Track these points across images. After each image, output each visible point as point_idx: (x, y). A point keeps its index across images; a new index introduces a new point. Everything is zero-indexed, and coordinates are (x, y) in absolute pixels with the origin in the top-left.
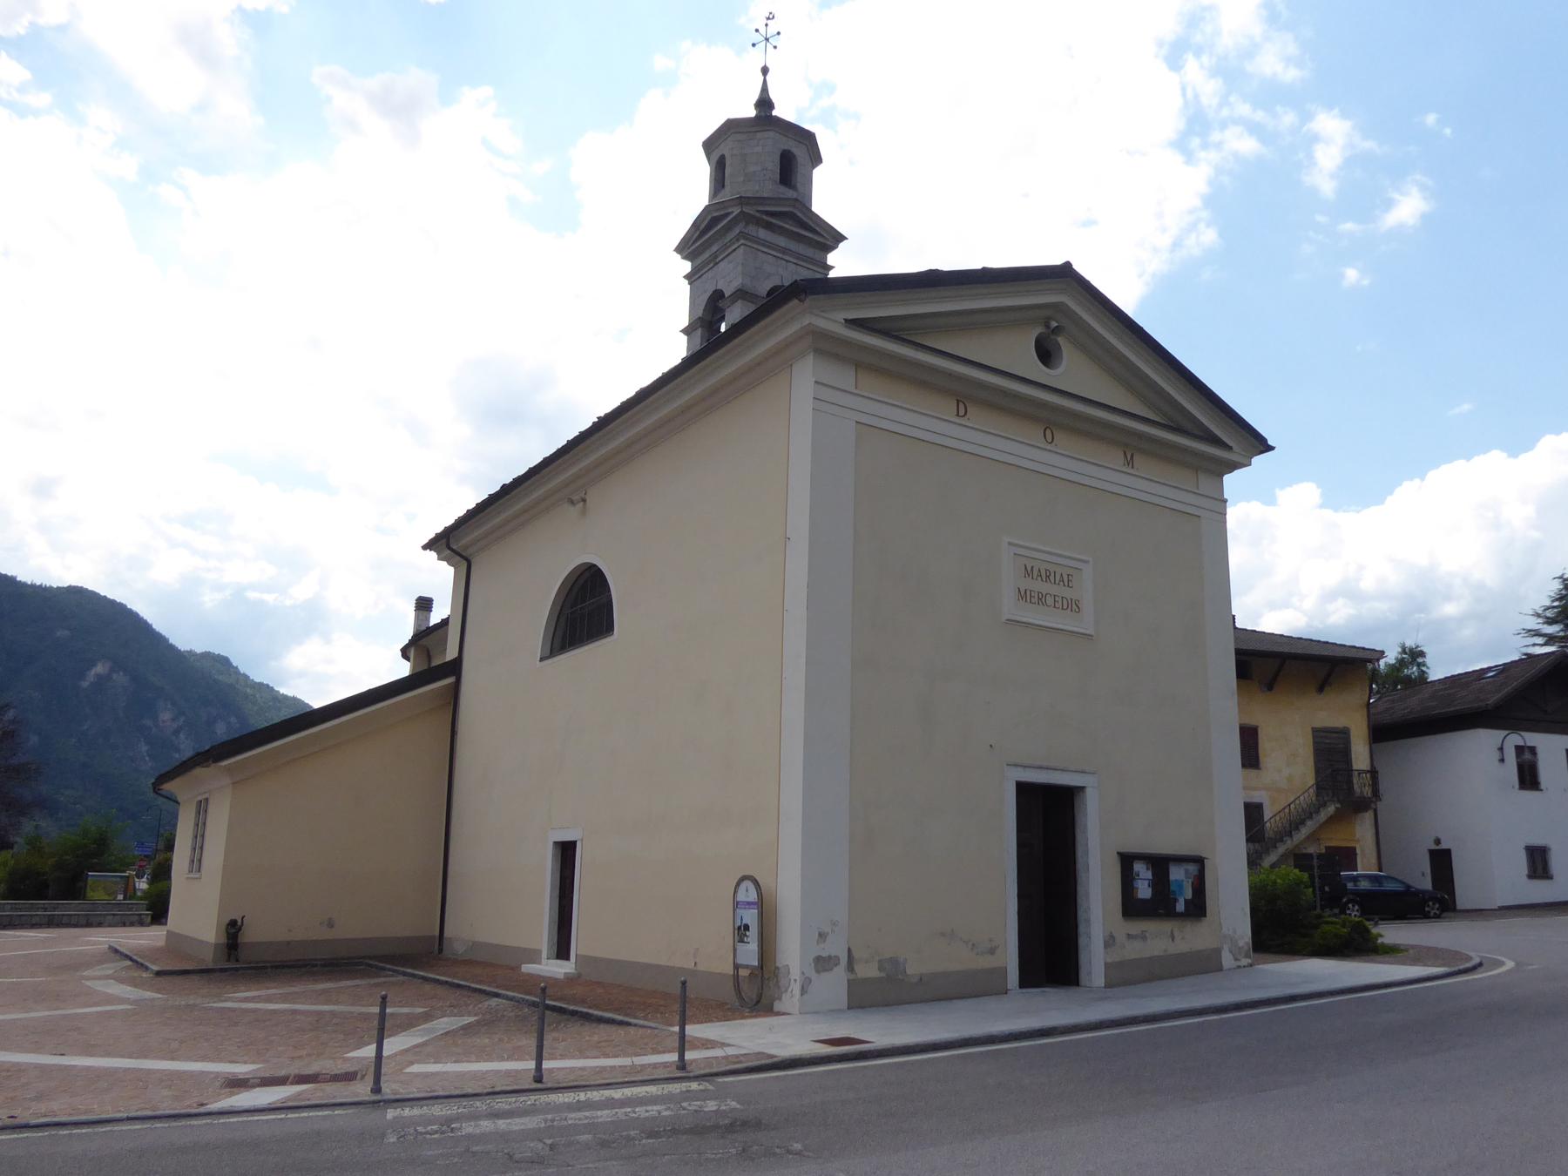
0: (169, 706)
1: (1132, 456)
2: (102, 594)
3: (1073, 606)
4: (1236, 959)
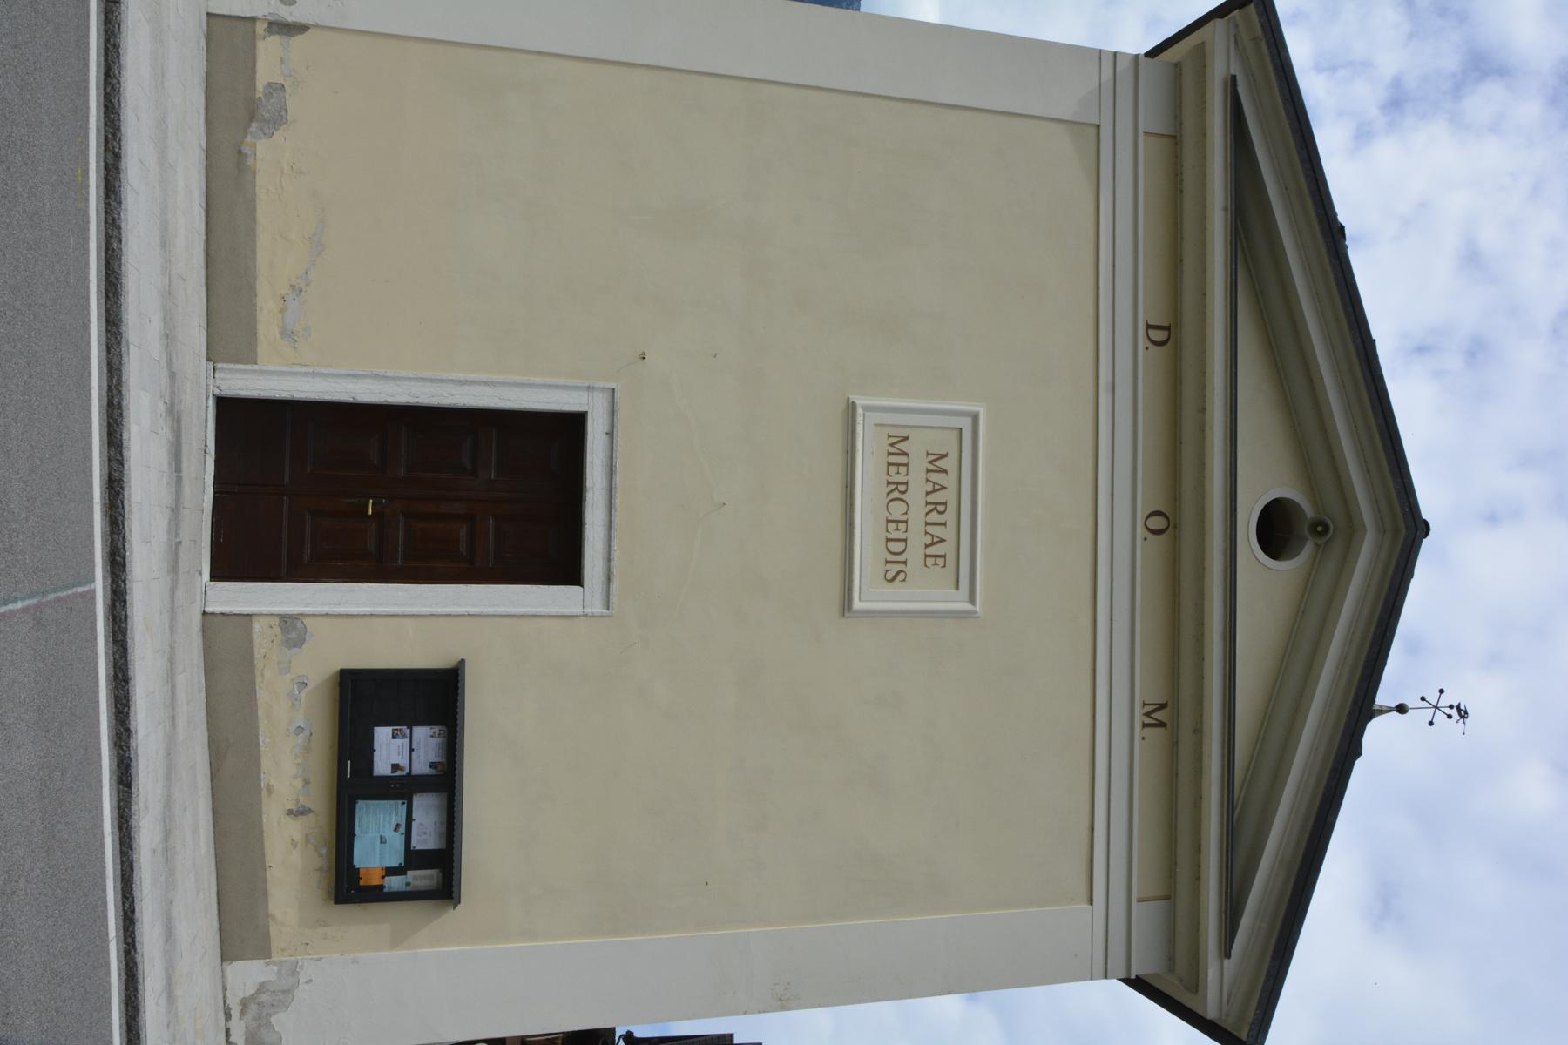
1: (1161, 724)
3: (895, 570)
4: (245, 1004)
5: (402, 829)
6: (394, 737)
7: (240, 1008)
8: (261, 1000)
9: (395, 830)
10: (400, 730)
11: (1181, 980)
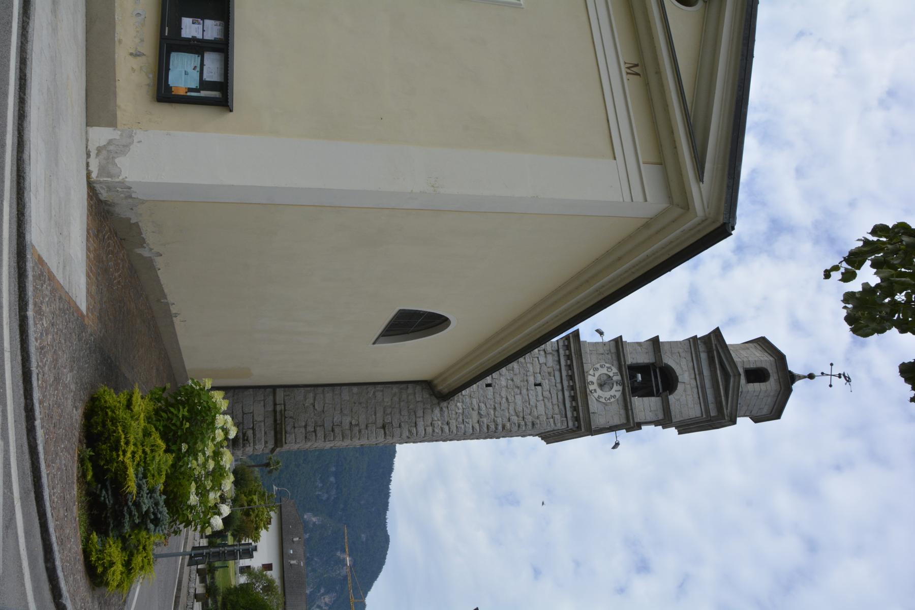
0: (333, 599)
2: (388, 552)
4: (99, 150)
5: (198, 69)
6: (193, 23)
7: (96, 152)
8: (109, 149)
9: (194, 69)
10: (197, 20)
11: (678, 205)
